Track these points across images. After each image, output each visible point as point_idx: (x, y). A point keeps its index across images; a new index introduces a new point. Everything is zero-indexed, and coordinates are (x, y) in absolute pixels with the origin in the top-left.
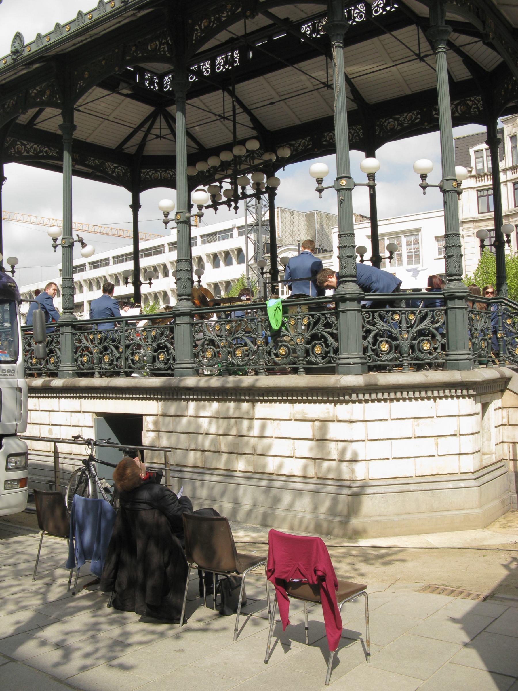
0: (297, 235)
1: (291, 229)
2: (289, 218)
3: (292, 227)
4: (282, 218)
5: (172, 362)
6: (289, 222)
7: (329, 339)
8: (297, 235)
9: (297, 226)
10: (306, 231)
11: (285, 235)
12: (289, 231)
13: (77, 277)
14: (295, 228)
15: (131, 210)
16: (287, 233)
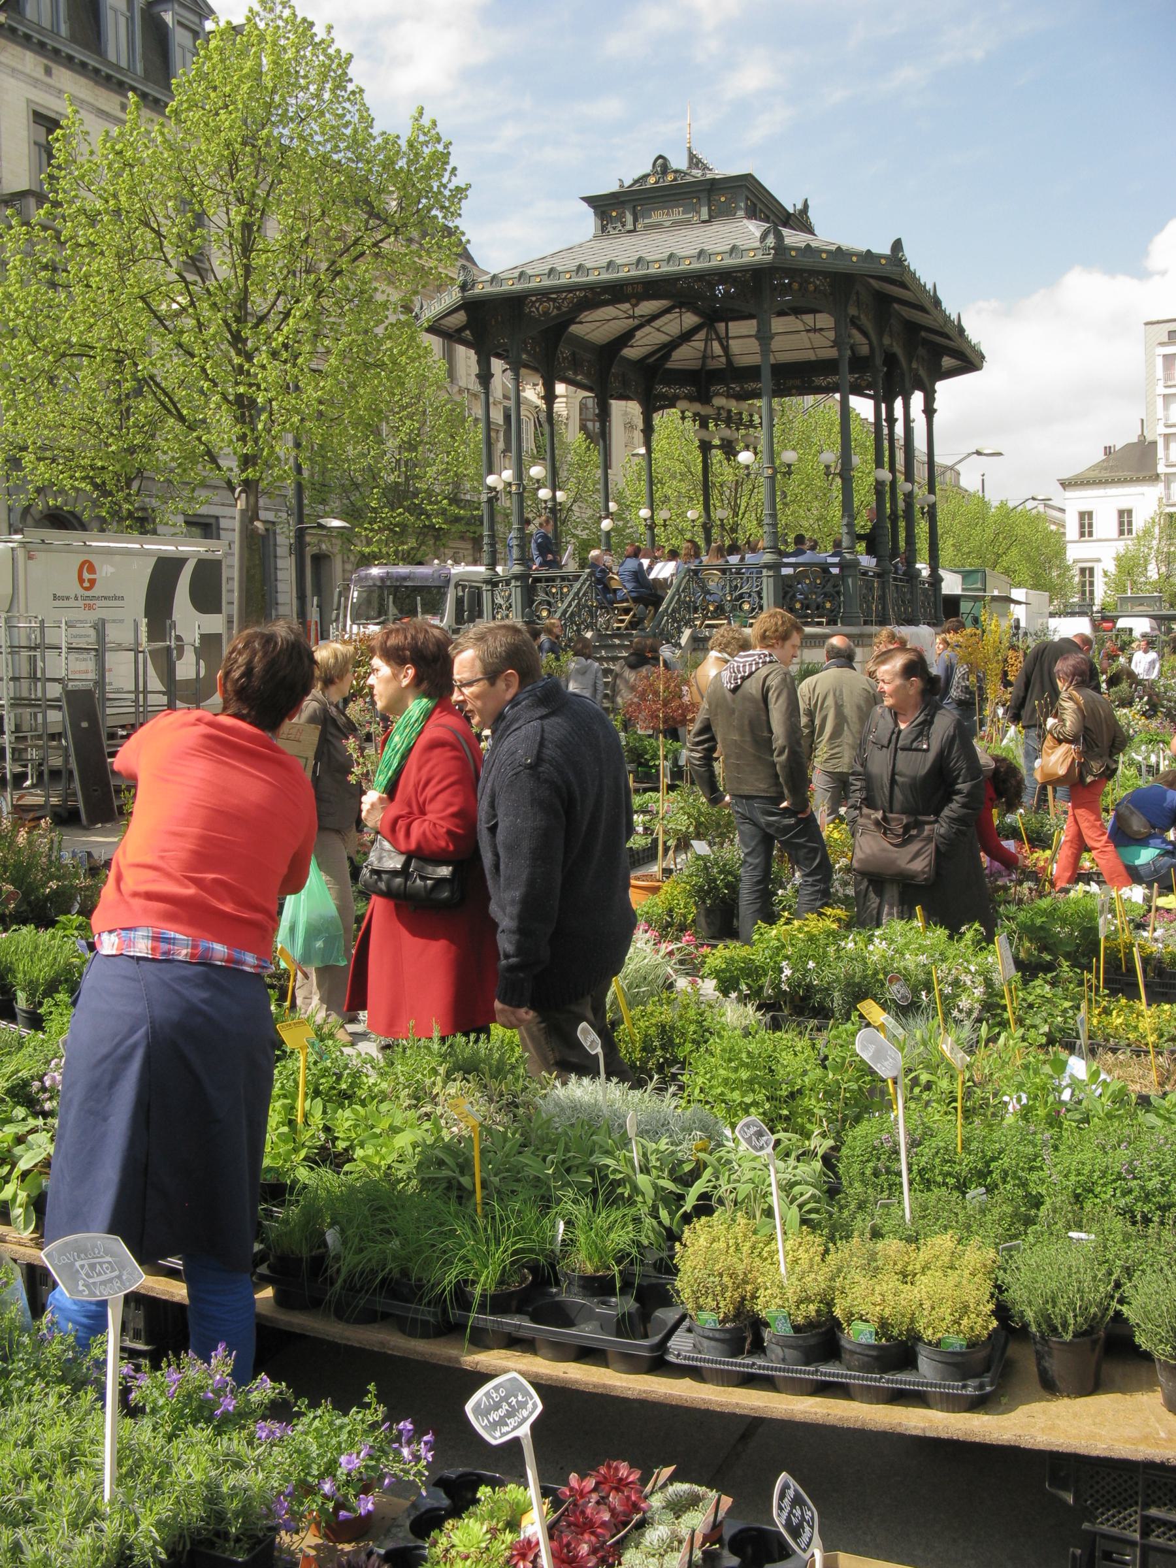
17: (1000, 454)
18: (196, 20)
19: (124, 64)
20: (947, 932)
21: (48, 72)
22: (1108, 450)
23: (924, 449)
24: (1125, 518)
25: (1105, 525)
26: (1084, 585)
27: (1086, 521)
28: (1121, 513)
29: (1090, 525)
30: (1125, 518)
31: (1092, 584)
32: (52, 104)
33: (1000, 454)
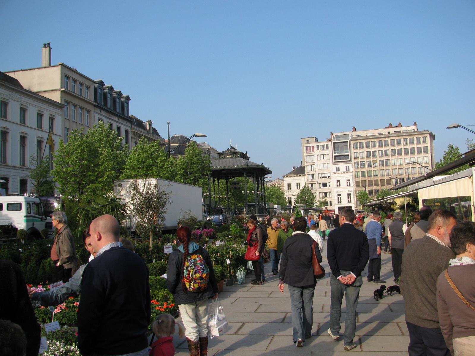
17: (448, 128)
18: (101, 87)
19: (86, 98)
20: (265, 265)
21: (101, 112)
22: (25, 217)
23: (112, 118)
24: (298, 185)
25: (294, 186)
26: (289, 201)
27: (289, 186)
28: (297, 184)
29: (290, 187)
30: (298, 185)
31: (291, 201)
32: (119, 125)
33: (448, 128)
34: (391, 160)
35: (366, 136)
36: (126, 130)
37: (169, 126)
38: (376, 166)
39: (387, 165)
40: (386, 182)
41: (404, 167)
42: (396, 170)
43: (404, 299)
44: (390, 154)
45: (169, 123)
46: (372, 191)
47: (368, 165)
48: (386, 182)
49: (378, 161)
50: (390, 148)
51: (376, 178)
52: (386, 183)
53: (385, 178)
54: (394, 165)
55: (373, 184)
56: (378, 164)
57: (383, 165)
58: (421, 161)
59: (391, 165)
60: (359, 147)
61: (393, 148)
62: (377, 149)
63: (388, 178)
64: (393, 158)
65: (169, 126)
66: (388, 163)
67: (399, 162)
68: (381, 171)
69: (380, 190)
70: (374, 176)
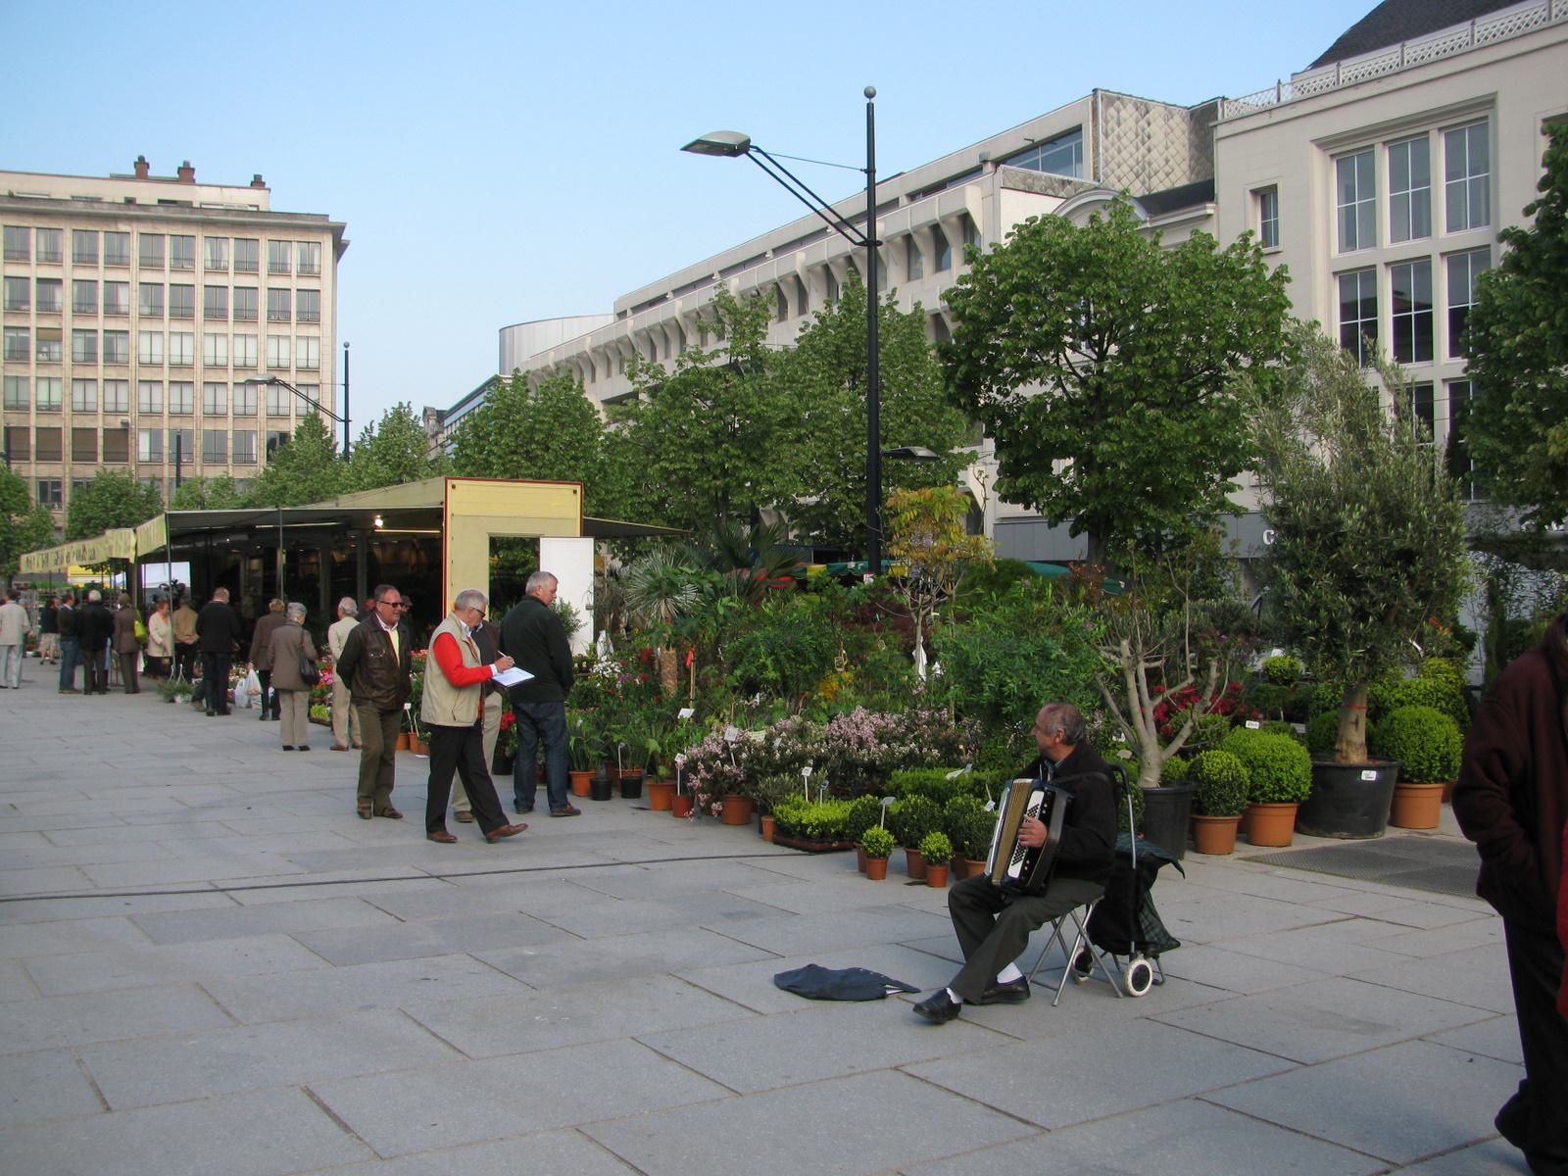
0: (1161, 175)
1: (1138, 155)
2: (1131, 123)
3: (1143, 150)
4: (1107, 122)
5: (1264, 695)
6: (1131, 136)
7: (1152, 709)
8: (1161, 175)
9: (1161, 148)
10: (1193, 162)
11: (1118, 172)
12: (1132, 162)
13: (885, 448)
14: (1154, 153)
15: (1486, 907)
16: (1125, 168)
34: (133, 334)
35: (11, 196)
36: (1080, 126)
37: (870, 108)
38: (56, 356)
39: (110, 357)
40: (100, 442)
41: (198, 377)
42: (90, 387)
43: (1060, 842)
44: (135, 304)
45: (870, 95)
46: (58, 484)
47: (11, 351)
48: (100, 442)
49: (67, 333)
50: (134, 275)
51: (48, 422)
52: (100, 450)
53: (34, 421)
54: (151, 364)
55: (33, 450)
56: (67, 351)
57: (90, 358)
58: (252, 353)
59: (133, 363)
60: (107, 256)
61: (150, 277)
62: (67, 272)
63: (116, 423)
64: (147, 326)
65: (870, 108)
66: (120, 350)
67: (240, 353)
68: (79, 388)
69: (67, 482)
70: (38, 408)
